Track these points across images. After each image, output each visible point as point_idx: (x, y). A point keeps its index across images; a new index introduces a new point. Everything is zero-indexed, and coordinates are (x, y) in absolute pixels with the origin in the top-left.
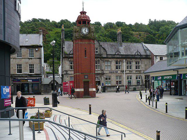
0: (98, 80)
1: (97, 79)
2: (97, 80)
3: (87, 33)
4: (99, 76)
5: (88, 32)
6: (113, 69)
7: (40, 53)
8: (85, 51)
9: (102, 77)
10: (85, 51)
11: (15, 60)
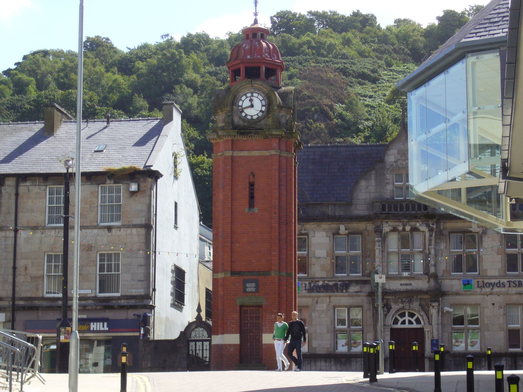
0: (415, 326)
1: (407, 318)
2: (410, 322)
3: (260, 114)
4: (415, 305)
5: (243, 114)
6: (490, 273)
7: (148, 202)
8: (252, 185)
9: (434, 312)
10: (252, 185)
11: (38, 234)
